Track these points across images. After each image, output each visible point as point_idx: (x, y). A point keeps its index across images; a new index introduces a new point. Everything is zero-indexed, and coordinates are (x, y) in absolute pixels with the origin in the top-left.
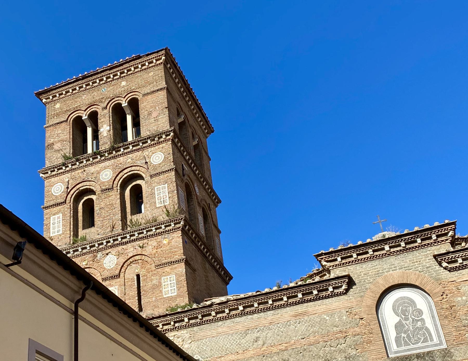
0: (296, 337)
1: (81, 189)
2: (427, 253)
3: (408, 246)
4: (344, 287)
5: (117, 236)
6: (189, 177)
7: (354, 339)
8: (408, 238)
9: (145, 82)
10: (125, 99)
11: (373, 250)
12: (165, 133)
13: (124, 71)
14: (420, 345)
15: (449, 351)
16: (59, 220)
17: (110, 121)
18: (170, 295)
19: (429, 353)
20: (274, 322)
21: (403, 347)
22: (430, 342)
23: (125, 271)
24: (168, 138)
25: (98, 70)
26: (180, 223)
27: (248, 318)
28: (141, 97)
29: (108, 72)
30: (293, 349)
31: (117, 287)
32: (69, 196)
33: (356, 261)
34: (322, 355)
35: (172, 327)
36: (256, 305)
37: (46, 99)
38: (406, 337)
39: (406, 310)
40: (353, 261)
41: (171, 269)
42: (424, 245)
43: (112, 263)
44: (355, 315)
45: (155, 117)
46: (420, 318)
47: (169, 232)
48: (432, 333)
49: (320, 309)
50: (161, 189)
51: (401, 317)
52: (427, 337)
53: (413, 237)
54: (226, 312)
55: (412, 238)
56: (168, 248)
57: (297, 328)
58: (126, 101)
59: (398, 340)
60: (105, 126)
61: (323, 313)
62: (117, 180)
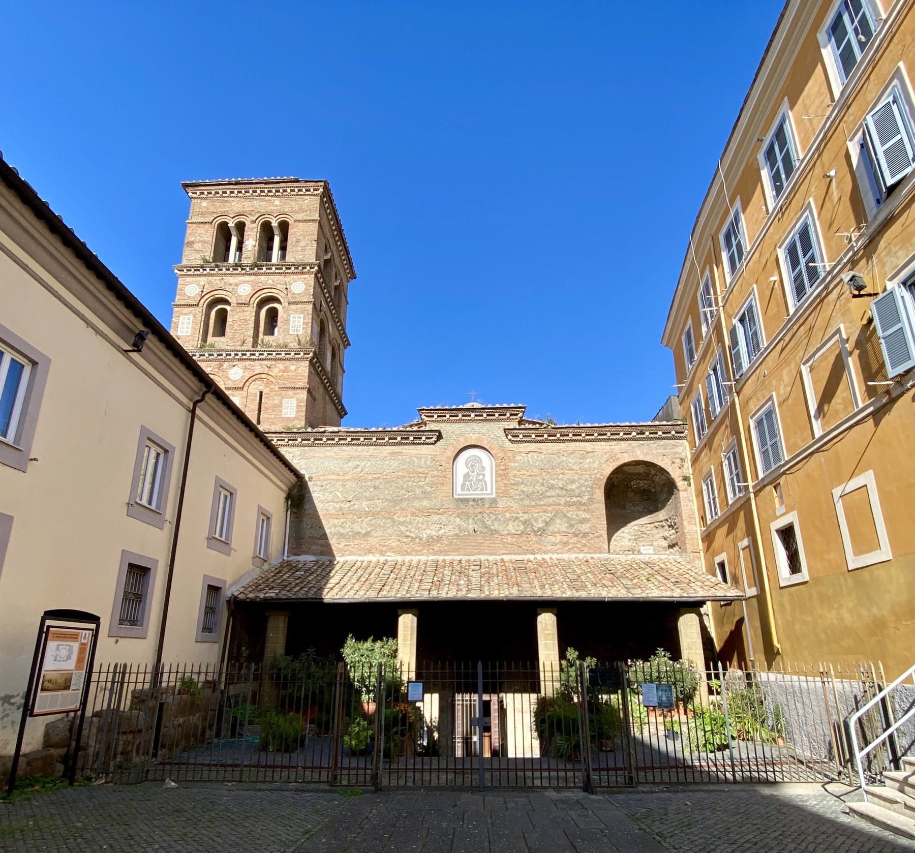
14: (477, 492)
19: (482, 499)
32: (203, 300)
59: (463, 486)
60: (251, 240)
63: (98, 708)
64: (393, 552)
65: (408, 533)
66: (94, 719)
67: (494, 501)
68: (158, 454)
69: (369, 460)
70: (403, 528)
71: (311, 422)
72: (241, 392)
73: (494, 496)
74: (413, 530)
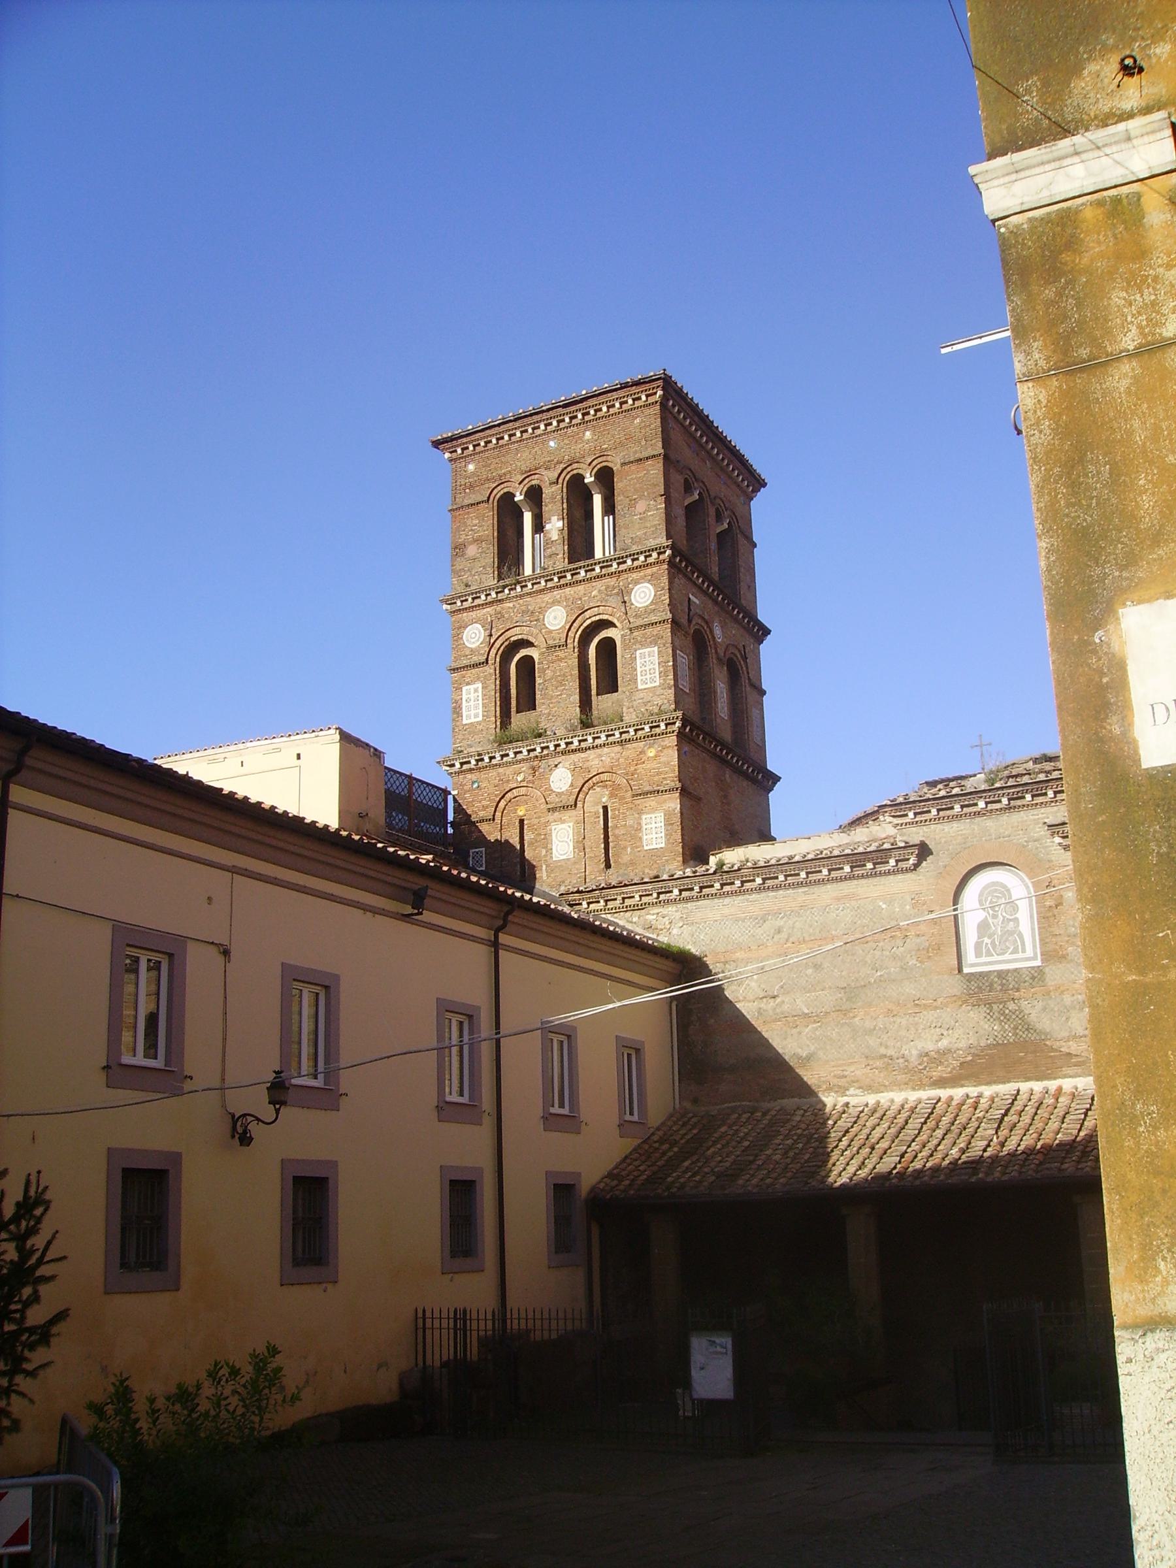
2: (1037, 817)
4: (911, 862)
6: (703, 618)
9: (627, 437)
10: (591, 467)
12: (656, 549)
14: (1007, 957)
17: (563, 509)
21: (984, 958)
22: (1021, 953)
25: (542, 407)
28: (619, 466)
31: (571, 824)
32: (493, 651)
33: (935, 819)
34: (869, 962)
35: (655, 901)
36: (781, 878)
37: (451, 452)
45: (641, 511)
50: (647, 656)
55: (1018, 792)
60: (554, 519)
63: (445, 1358)
65: (883, 1051)
66: (443, 1370)
67: (1037, 975)
68: (461, 1023)
70: (872, 1041)
71: (696, 853)
73: (1038, 963)
74: (891, 1043)
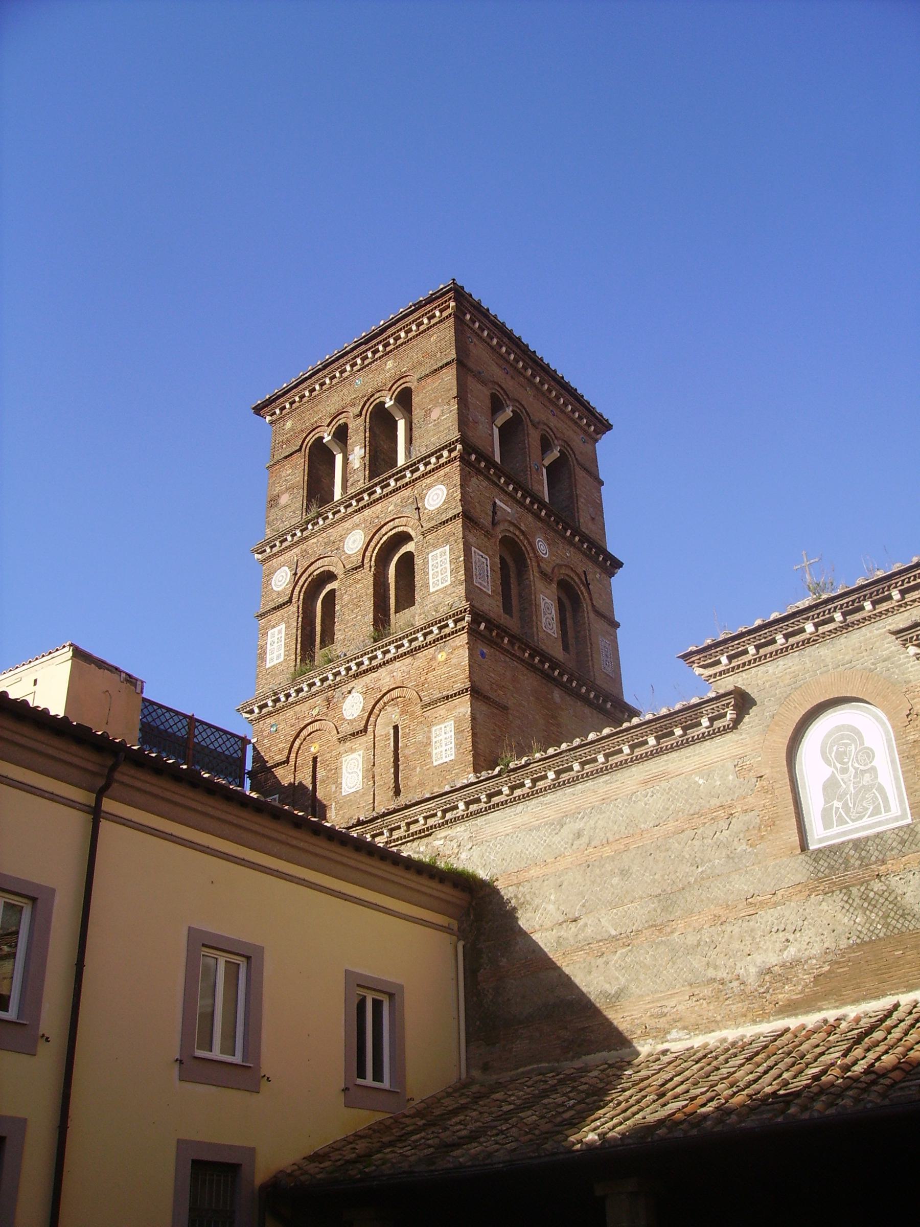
0: (645, 822)
1: (315, 573)
3: (850, 619)
5: (362, 656)
7: (745, 818)
8: (847, 603)
11: (783, 634)
13: (411, 328)
14: (866, 821)
15: (913, 830)
16: (279, 636)
17: (365, 438)
18: (445, 760)
19: (877, 835)
20: (608, 798)
23: (376, 721)
24: (453, 455)
26: (463, 619)
27: (565, 794)
29: (364, 347)
30: (638, 847)
31: (361, 752)
32: (297, 589)
34: (687, 856)
36: (576, 767)
37: (271, 415)
38: (840, 807)
39: (845, 752)
40: (750, 662)
41: (447, 710)
42: (879, 613)
43: (355, 707)
44: (750, 771)
46: (869, 766)
47: (448, 638)
48: (888, 795)
49: (689, 764)
51: (835, 767)
52: (879, 804)
53: (855, 600)
54: (527, 786)
55: (853, 601)
56: (445, 670)
57: (647, 807)
58: (392, 396)
59: (826, 815)
61: (694, 773)
62: (370, 549)
64: (685, 1028)
65: (711, 973)
69: (601, 812)
70: (697, 962)
72: (364, 739)
74: (720, 962)
